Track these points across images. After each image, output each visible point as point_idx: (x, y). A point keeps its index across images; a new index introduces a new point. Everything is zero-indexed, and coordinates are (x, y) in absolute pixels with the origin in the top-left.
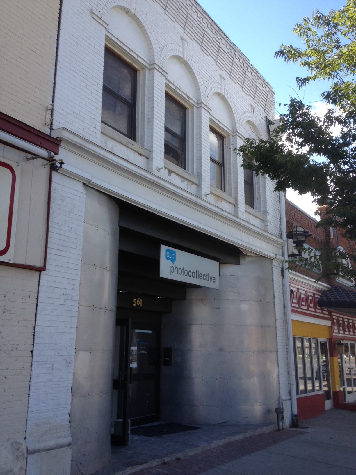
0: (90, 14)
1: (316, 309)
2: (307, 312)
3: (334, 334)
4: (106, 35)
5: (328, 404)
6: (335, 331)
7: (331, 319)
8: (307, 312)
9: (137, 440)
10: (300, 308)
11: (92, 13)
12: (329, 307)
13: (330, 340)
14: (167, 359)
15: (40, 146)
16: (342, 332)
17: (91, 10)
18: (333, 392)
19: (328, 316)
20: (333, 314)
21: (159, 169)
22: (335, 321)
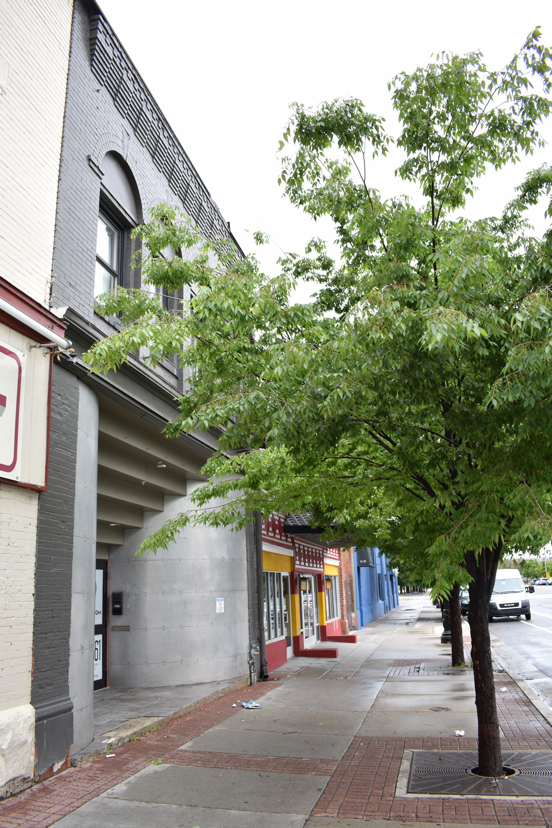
0: (86, 163)
1: (281, 536)
2: (274, 540)
3: (296, 566)
4: (101, 192)
5: (290, 651)
6: (298, 562)
7: (293, 547)
8: (274, 540)
9: (426, 368)
10: (268, 536)
11: (90, 160)
12: (292, 533)
13: (292, 574)
14: (118, 606)
15: (263, 608)
16: (303, 563)
17: (89, 156)
18: (294, 637)
19: (291, 544)
20: (295, 541)
21: (145, 358)
22: (297, 550)
